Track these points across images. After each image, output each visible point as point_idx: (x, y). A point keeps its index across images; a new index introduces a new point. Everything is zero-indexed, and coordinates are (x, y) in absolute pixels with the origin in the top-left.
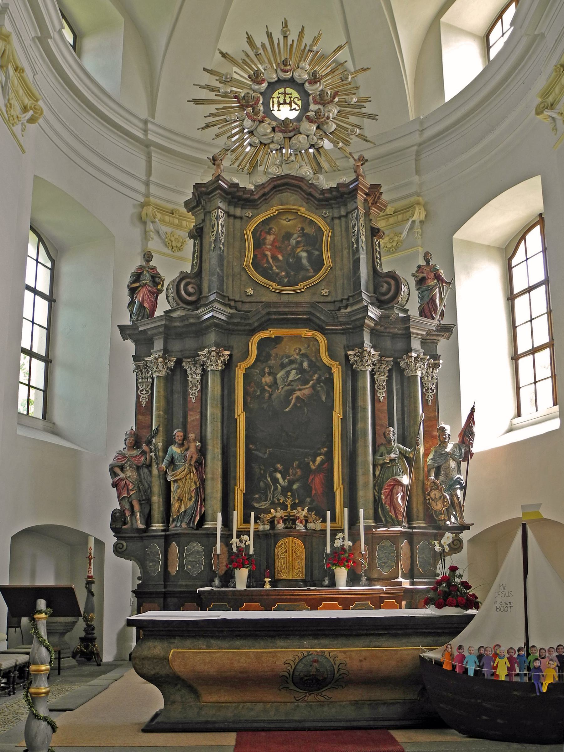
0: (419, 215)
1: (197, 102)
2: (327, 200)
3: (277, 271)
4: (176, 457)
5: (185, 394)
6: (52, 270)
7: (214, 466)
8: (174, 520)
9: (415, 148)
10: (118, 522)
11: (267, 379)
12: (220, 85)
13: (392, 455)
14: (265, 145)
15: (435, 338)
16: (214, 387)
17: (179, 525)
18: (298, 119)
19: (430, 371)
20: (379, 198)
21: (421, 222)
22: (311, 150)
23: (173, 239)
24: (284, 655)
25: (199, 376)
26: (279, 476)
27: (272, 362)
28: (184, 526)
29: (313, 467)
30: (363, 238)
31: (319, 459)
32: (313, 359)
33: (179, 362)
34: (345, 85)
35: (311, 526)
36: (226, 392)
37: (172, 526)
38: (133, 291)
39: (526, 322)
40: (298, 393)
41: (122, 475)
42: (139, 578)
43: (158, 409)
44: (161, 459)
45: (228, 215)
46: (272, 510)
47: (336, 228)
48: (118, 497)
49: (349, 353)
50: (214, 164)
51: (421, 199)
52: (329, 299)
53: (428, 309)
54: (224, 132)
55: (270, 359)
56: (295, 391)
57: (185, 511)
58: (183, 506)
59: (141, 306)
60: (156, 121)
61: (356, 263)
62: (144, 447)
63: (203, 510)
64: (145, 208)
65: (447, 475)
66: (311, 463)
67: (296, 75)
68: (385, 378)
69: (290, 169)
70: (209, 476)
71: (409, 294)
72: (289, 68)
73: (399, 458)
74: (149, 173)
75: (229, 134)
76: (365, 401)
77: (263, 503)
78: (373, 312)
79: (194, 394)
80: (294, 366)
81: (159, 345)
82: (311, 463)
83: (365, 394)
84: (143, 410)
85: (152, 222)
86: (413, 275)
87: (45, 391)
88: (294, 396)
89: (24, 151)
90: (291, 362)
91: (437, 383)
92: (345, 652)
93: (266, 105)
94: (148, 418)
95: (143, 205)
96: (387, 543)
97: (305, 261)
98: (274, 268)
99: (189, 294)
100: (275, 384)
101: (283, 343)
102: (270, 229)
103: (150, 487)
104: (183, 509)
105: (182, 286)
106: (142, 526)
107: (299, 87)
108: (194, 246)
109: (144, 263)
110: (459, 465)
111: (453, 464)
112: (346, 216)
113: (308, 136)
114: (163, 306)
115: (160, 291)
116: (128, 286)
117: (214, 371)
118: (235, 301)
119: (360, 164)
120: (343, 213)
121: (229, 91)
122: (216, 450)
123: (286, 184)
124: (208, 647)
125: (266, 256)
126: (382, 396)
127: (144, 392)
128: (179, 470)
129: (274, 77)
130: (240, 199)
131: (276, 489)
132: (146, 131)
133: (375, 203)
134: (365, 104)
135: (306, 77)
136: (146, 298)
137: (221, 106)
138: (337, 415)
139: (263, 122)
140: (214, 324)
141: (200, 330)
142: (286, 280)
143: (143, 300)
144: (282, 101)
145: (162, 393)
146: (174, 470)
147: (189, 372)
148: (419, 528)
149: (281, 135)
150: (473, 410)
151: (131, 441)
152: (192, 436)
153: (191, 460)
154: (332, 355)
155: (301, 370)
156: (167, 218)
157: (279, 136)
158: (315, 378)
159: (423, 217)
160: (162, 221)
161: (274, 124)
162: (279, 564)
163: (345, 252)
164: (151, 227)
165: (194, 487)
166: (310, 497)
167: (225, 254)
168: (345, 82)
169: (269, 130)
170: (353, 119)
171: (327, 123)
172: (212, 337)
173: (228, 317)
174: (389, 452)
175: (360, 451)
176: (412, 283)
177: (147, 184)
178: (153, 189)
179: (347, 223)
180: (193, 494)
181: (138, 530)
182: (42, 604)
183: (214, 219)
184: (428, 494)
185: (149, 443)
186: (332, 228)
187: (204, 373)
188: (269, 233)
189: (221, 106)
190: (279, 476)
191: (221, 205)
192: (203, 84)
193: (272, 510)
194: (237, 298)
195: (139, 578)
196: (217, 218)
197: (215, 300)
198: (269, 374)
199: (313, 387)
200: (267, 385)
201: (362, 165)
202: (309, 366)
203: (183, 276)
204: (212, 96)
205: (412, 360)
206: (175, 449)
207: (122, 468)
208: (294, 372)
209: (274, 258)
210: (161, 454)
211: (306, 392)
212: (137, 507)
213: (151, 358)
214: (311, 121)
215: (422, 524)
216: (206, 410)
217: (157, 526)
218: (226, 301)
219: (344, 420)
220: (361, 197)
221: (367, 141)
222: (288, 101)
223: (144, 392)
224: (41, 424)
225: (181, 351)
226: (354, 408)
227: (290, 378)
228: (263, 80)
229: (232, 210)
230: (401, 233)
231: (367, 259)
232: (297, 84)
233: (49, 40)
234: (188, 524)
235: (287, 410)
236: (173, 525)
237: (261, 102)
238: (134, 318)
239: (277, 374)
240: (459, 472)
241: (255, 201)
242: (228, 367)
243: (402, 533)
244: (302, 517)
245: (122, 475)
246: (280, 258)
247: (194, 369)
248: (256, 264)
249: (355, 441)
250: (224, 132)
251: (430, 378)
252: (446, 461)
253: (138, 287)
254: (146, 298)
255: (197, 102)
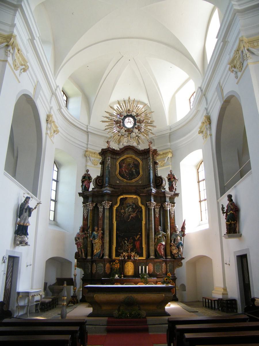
0: (170, 155)
1: (103, 122)
2: (141, 153)
3: (126, 176)
4: (95, 235)
5: (98, 215)
6: (58, 172)
7: (107, 239)
8: (94, 256)
9: (169, 134)
10: (77, 256)
11: (123, 211)
12: (110, 116)
13: (160, 235)
14: (123, 135)
15: (174, 197)
16: (107, 214)
17: (96, 257)
18: (133, 127)
19: (172, 207)
20: (157, 153)
21: (171, 157)
22: (137, 137)
23: (95, 162)
24: (122, 297)
25: (102, 209)
26: (126, 242)
27: (124, 205)
28: (97, 258)
29: (136, 239)
30: (152, 166)
31: (138, 236)
32: (137, 205)
33: (96, 205)
34: (147, 117)
35: (136, 258)
36: (110, 215)
37: (94, 258)
38: (83, 182)
39: (68, 313)
40: (132, 215)
41: (79, 241)
42: (83, 275)
43: (90, 220)
44: (91, 236)
45: (112, 158)
46: (124, 253)
47: (144, 162)
48: (77, 248)
49: (147, 203)
50: (107, 143)
51: (170, 150)
52: (141, 185)
53: (171, 188)
54: (111, 131)
55: (123, 205)
56: (131, 214)
57: (98, 253)
58: (97, 251)
59: (85, 186)
60: (90, 125)
61: (150, 173)
62: (86, 232)
63: (103, 252)
64: (87, 152)
65: (177, 241)
66: (136, 238)
67: (132, 114)
68: (158, 210)
69: (130, 144)
70: (105, 242)
71: (165, 183)
72: (130, 112)
73: (162, 236)
74: (88, 142)
75: (112, 132)
76: (152, 218)
77: (121, 251)
78: (154, 191)
79: (101, 215)
80: (131, 207)
81: (90, 199)
82: (136, 238)
83: (152, 216)
84: (85, 219)
85: (89, 157)
86: (167, 177)
87: (54, 211)
88: (131, 216)
89: (53, 143)
90: (130, 205)
91: (174, 212)
92: (137, 296)
93: (123, 123)
94: (87, 222)
95: (86, 151)
96: (158, 264)
97: (134, 173)
98: (125, 175)
99: (100, 183)
100: (125, 213)
101: (127, 199)
102: (124, 162)
103: (87, 245)
104: (97, 252)
105: (98, 181)
106: (84, 257)
107: (133, 117)
108: (101, 167)
109: (86, 173)
110: (181, 238)
111: (179, 238)
112: (147, 158)
113: (135, 133)
114: (92, 186)
115: (91, 182)
116: (81, 180)
117: (107, 208)
118: (114, 185)
119: (150, 144)
120: (146, 158)
121: (112, 118)
122: (107, 233)
123: (128, 148)
124: (104, 294)
125: (123, 171)
126: (157, 216)
127: (86, 214)
128: (96, 240)
129: (126, 114)
130: (115, 153)
131: (125, 246)
132: (87, 128)
133: (155, 154)
134: (153, 123)
135: (135, 114)
136: (87, 184)
137: (110, 123)
138: (144, 222)
139: (122, 128)
140: (107, 194)
141: (103, 195)
142: (129, 178)
143: (86, 185)
144: (128, 122)
145: (91, 215)
146: (94, 239)
147: (99, 208)
148: (169, 259)
149: (127, 133)
150: (185, 220)
151: (82, 230)
152: (100, 229)
153: (100, 237)
154: (142, 203)
155: (133, 208)
156: (93, 155)
157: (127, 133)
158: (137, 211)
159: (171, 156)
160: (92, 156)
161: (126, 129)
162: (126, 270)
163: (146, 170)
164: (88, 158)
165: (100, 245)
166: (136, 248)
167: (110, 170)
168: (147, 116)
169: (124, 131)
170: (149, 127)
171: (141, 129)
172: (106, 198)
173: (111, 192)
174: (159, 234)
175: (150, 234)
176: (167, 180)
177: (87, 144)
178: (89, 146)
179: (147, 160)
180: (100, 248)
181: (83, 259)
182: (65, 282)
183: (107, 159)
184: (172, 248)
185: (87, 231)
186: (143, 162)
187: (104, 209)
188: (124, 164)
189: (110, 123)
190: (126, 242)
191: (109, 155)
192: (105, 116)
193: (124, 253)
194: (114, 184)
195: (83, 275)
196: (108, 160)
197: (107, 186)
198: (123, 209)
199: (136, 213)
200: (123, 213)
201: (151, 144)
202: (135, 207)
203: (98, 177)
204: (107, 120)
205: (166, 205)
206: (95, 233)
207: (79, 239)
208: (131, 208)
209: (125, 171)
210: (91, 234)
211: (134, 215)
212: (83, 251)
213: (88, 204)
214: (136, 128)
215: (170, 257)
216: (104, 220)
217: (89, 258)
218: (111, 186)
219: (146, 224)
220: (151, 153)
221: (153, 134)
222: (130, 122)
223: (86, 214)
224: (53, 222)
225: (97, 201)
226: (149, 220)
227: (129, 211)
228: (122, 116)
229: (113, 156)
230: (165, 161)
231: (153, 173)
232: (133, 116)
233: (62, 109)
234: (98, 257)
235: (129, 220)
236: (94, 257)
237: (122, 122)
238: (83, 190)
239: (125, 209)
240: (181, 240)
241: (119, 153)
242: (111, 207)
243: (163, 260)
244: (133, 255)
245: (79, 241)
246: (127, 171)
247: (101, 207)
248: (120, 173)
249: (149, 230)
250: (111, 131)
251: (172, 210)
252: (177, 237)
253: (84, 181)
254: (87, 184)
255: (103, 122)
